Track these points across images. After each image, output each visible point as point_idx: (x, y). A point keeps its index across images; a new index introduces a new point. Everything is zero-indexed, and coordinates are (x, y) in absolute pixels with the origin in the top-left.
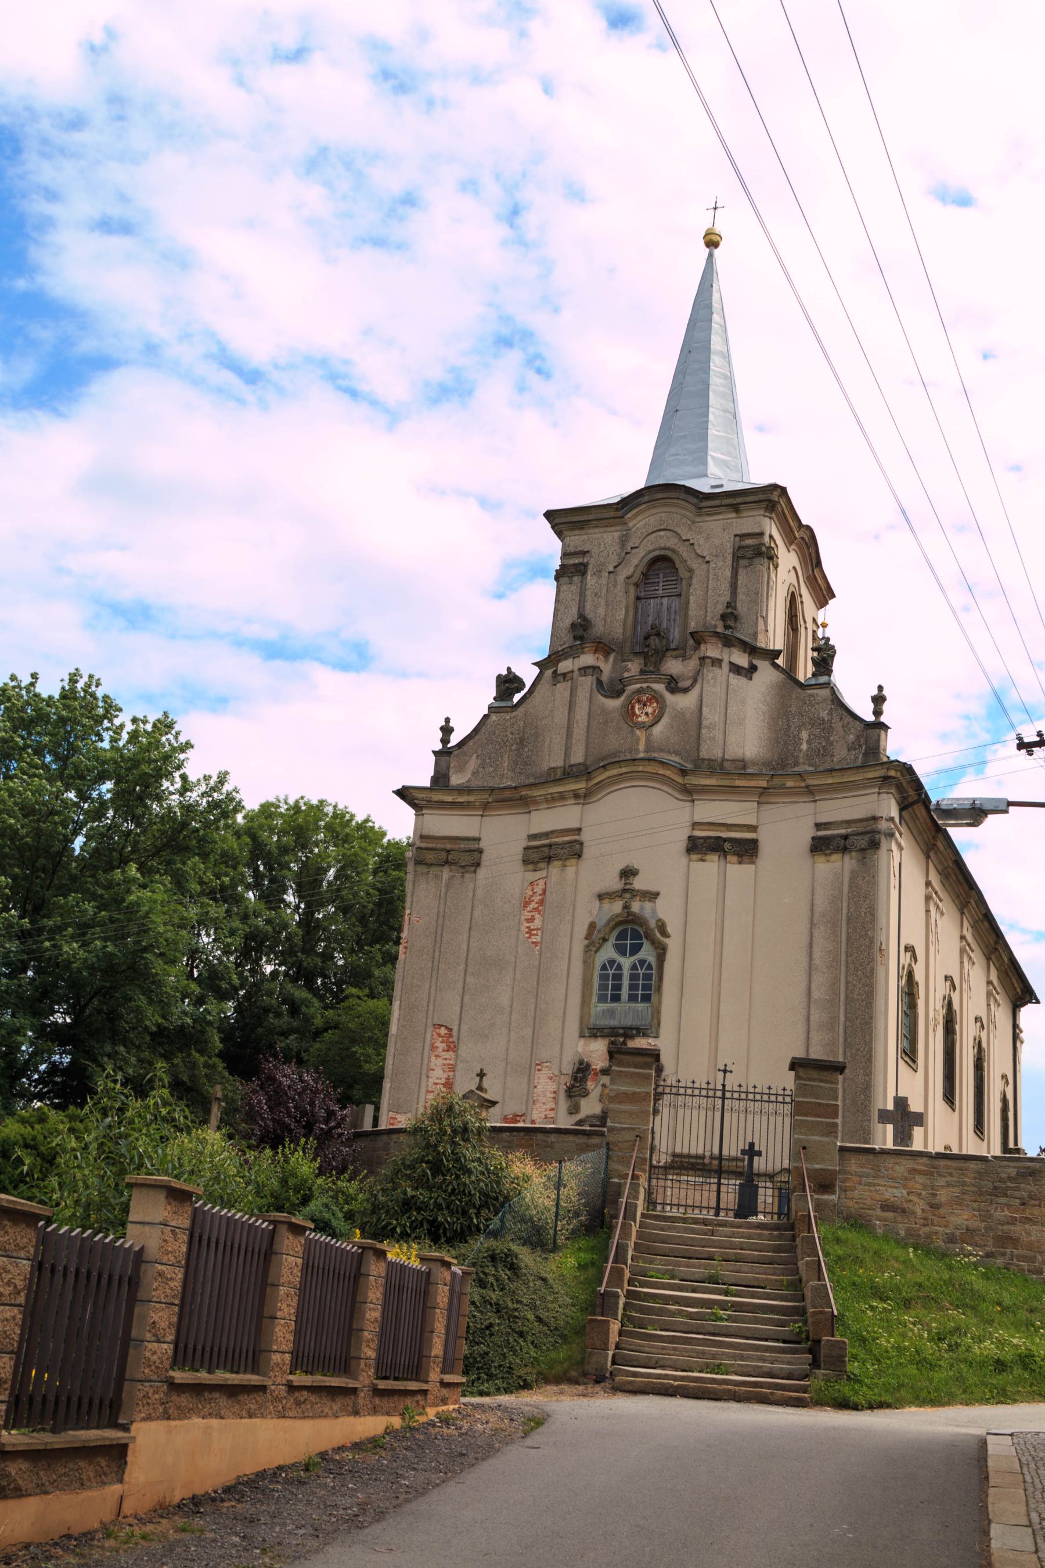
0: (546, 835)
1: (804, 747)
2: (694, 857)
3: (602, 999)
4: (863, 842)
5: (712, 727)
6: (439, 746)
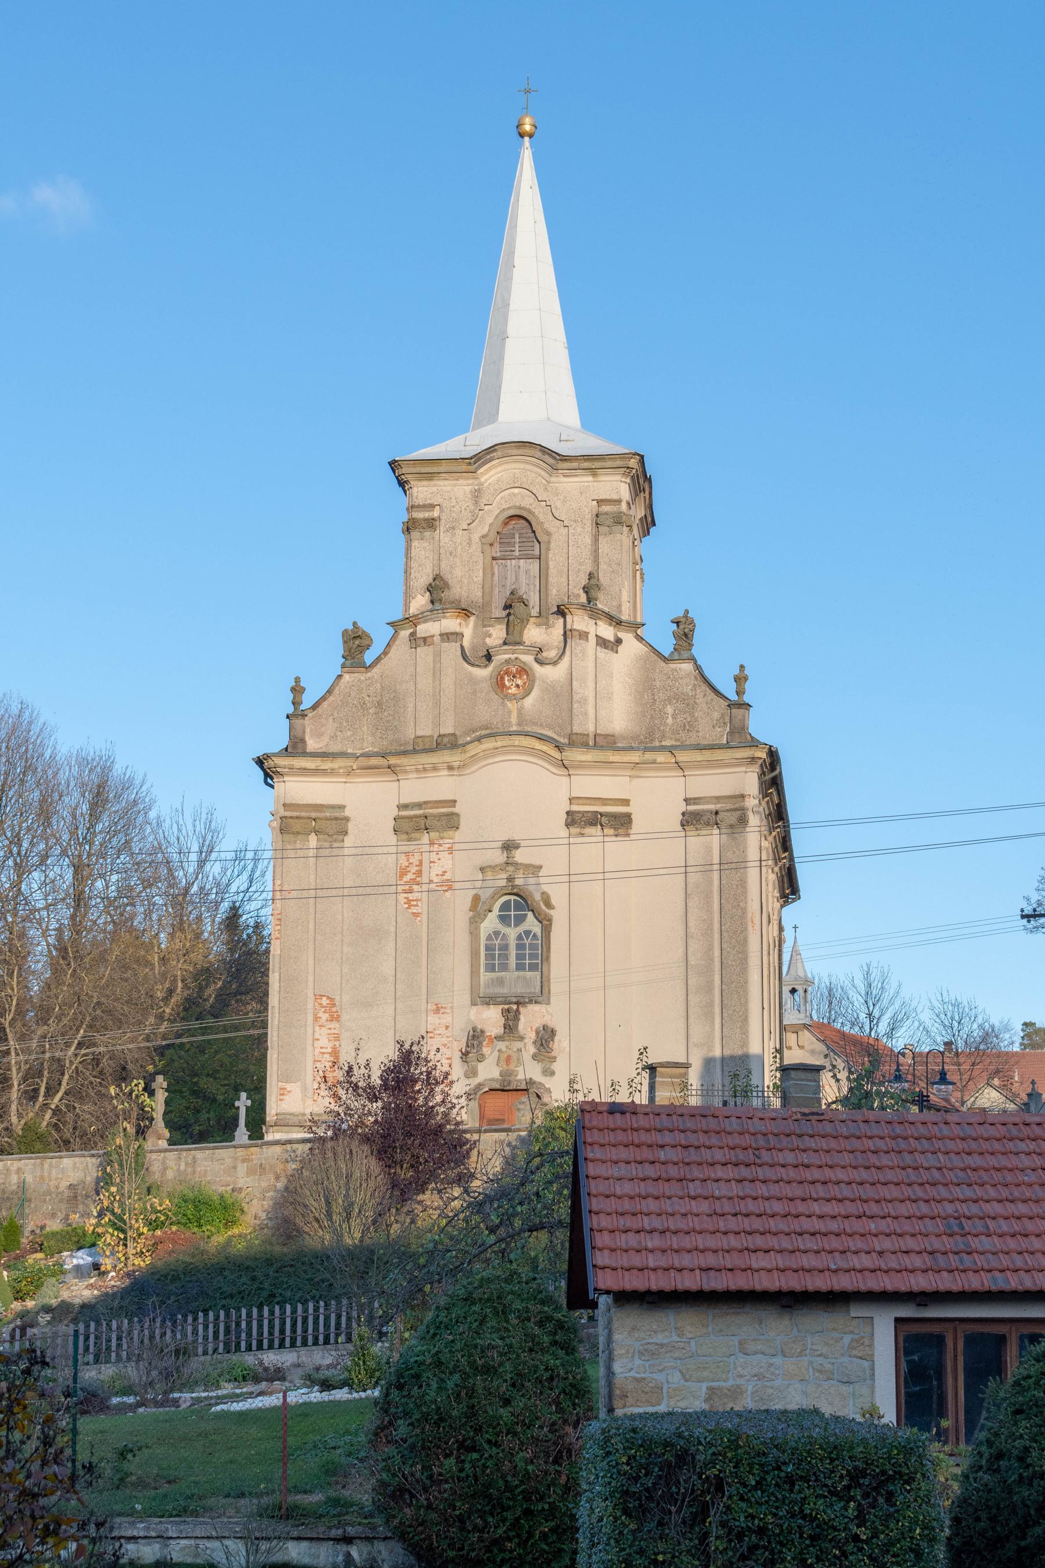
0: (419, 805)
1: (670, 721)
2: (574, 830)
3: (491, 968)
4: (732, 818)
5: (584, 701)
6: (291, 710)
